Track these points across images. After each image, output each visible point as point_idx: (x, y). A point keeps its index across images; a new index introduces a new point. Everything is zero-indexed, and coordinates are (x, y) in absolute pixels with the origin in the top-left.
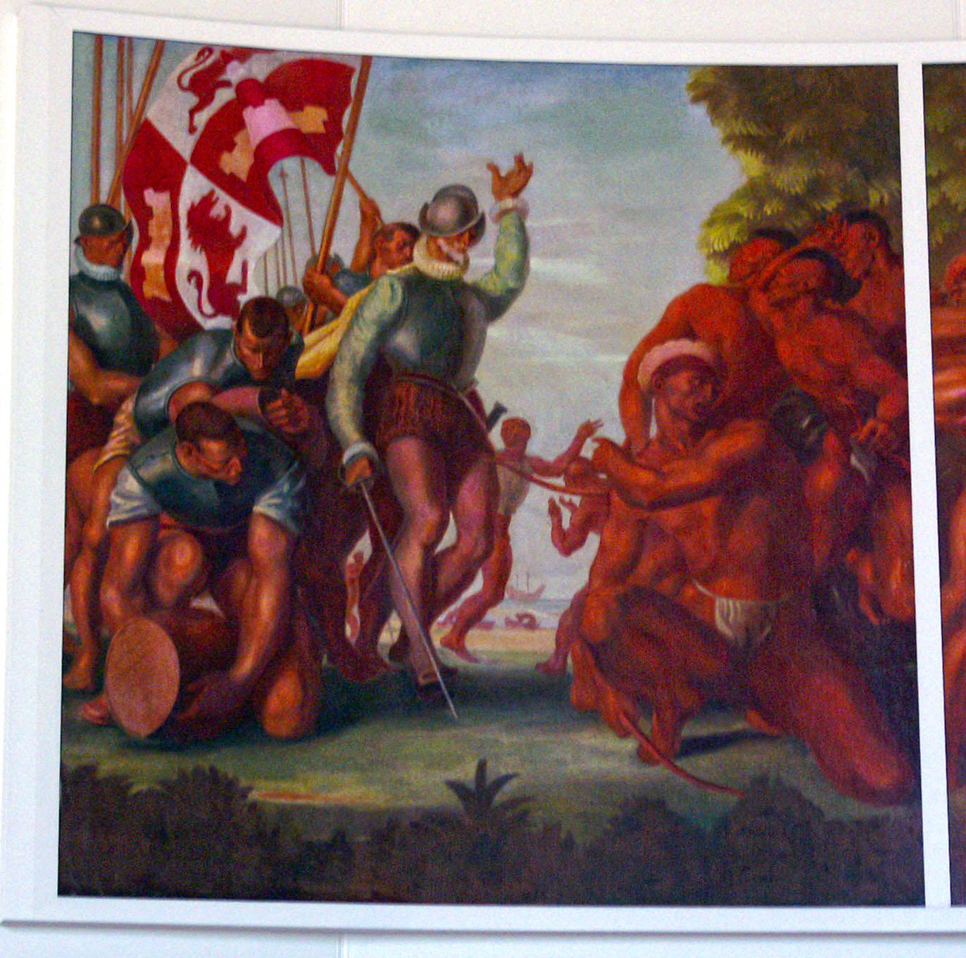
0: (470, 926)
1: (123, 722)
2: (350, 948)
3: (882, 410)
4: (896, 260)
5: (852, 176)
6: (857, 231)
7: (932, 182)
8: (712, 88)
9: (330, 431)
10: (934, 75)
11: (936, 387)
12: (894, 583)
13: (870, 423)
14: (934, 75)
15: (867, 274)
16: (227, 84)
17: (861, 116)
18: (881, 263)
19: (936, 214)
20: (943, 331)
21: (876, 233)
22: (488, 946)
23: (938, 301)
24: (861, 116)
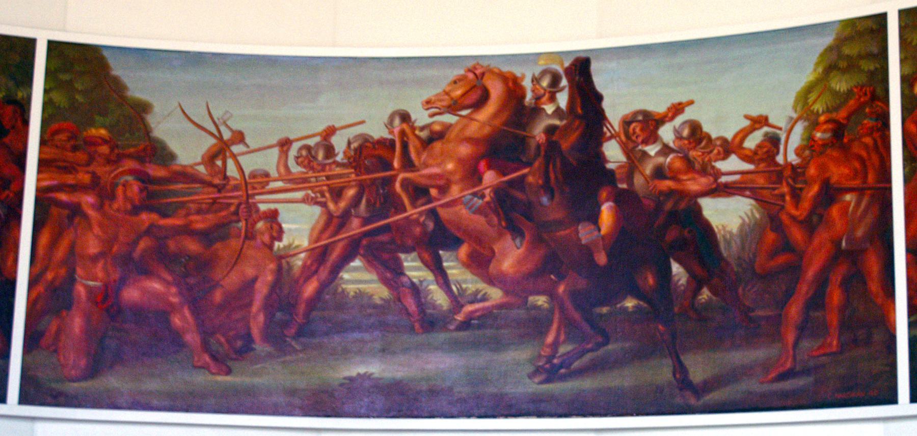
0: (67, 416)
1: (626, 384)
2: (40, 426)
3: (13, 186)
4: (26, 123)
5: (11, 84)
6: (10, 109)
7: (46, 91)
8: (771, 236)
9: (189, 234)
10: (53, 46)
11: (38, 180)
12: (9, 263)
13: (7, 192)
14: (53, 46)
15: (13, 127)
16: (607, 200)
17: (18, 58)
18: (19, 123)
19: (46, 104)
20: (44, 156)
21: (19, 111)
22: (216, 430)
23: (43, 143)
24: (18, 58)
